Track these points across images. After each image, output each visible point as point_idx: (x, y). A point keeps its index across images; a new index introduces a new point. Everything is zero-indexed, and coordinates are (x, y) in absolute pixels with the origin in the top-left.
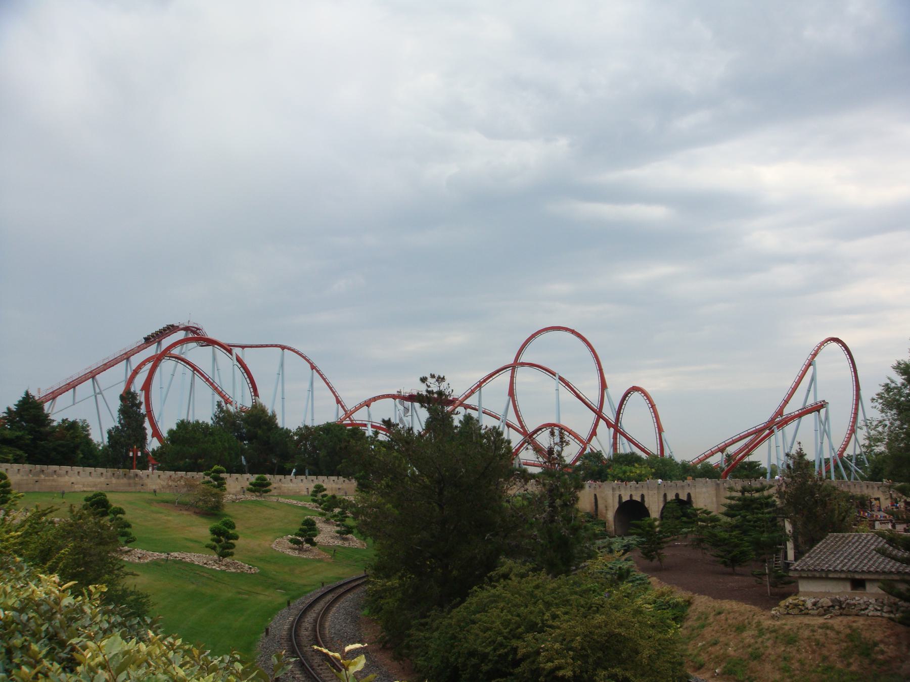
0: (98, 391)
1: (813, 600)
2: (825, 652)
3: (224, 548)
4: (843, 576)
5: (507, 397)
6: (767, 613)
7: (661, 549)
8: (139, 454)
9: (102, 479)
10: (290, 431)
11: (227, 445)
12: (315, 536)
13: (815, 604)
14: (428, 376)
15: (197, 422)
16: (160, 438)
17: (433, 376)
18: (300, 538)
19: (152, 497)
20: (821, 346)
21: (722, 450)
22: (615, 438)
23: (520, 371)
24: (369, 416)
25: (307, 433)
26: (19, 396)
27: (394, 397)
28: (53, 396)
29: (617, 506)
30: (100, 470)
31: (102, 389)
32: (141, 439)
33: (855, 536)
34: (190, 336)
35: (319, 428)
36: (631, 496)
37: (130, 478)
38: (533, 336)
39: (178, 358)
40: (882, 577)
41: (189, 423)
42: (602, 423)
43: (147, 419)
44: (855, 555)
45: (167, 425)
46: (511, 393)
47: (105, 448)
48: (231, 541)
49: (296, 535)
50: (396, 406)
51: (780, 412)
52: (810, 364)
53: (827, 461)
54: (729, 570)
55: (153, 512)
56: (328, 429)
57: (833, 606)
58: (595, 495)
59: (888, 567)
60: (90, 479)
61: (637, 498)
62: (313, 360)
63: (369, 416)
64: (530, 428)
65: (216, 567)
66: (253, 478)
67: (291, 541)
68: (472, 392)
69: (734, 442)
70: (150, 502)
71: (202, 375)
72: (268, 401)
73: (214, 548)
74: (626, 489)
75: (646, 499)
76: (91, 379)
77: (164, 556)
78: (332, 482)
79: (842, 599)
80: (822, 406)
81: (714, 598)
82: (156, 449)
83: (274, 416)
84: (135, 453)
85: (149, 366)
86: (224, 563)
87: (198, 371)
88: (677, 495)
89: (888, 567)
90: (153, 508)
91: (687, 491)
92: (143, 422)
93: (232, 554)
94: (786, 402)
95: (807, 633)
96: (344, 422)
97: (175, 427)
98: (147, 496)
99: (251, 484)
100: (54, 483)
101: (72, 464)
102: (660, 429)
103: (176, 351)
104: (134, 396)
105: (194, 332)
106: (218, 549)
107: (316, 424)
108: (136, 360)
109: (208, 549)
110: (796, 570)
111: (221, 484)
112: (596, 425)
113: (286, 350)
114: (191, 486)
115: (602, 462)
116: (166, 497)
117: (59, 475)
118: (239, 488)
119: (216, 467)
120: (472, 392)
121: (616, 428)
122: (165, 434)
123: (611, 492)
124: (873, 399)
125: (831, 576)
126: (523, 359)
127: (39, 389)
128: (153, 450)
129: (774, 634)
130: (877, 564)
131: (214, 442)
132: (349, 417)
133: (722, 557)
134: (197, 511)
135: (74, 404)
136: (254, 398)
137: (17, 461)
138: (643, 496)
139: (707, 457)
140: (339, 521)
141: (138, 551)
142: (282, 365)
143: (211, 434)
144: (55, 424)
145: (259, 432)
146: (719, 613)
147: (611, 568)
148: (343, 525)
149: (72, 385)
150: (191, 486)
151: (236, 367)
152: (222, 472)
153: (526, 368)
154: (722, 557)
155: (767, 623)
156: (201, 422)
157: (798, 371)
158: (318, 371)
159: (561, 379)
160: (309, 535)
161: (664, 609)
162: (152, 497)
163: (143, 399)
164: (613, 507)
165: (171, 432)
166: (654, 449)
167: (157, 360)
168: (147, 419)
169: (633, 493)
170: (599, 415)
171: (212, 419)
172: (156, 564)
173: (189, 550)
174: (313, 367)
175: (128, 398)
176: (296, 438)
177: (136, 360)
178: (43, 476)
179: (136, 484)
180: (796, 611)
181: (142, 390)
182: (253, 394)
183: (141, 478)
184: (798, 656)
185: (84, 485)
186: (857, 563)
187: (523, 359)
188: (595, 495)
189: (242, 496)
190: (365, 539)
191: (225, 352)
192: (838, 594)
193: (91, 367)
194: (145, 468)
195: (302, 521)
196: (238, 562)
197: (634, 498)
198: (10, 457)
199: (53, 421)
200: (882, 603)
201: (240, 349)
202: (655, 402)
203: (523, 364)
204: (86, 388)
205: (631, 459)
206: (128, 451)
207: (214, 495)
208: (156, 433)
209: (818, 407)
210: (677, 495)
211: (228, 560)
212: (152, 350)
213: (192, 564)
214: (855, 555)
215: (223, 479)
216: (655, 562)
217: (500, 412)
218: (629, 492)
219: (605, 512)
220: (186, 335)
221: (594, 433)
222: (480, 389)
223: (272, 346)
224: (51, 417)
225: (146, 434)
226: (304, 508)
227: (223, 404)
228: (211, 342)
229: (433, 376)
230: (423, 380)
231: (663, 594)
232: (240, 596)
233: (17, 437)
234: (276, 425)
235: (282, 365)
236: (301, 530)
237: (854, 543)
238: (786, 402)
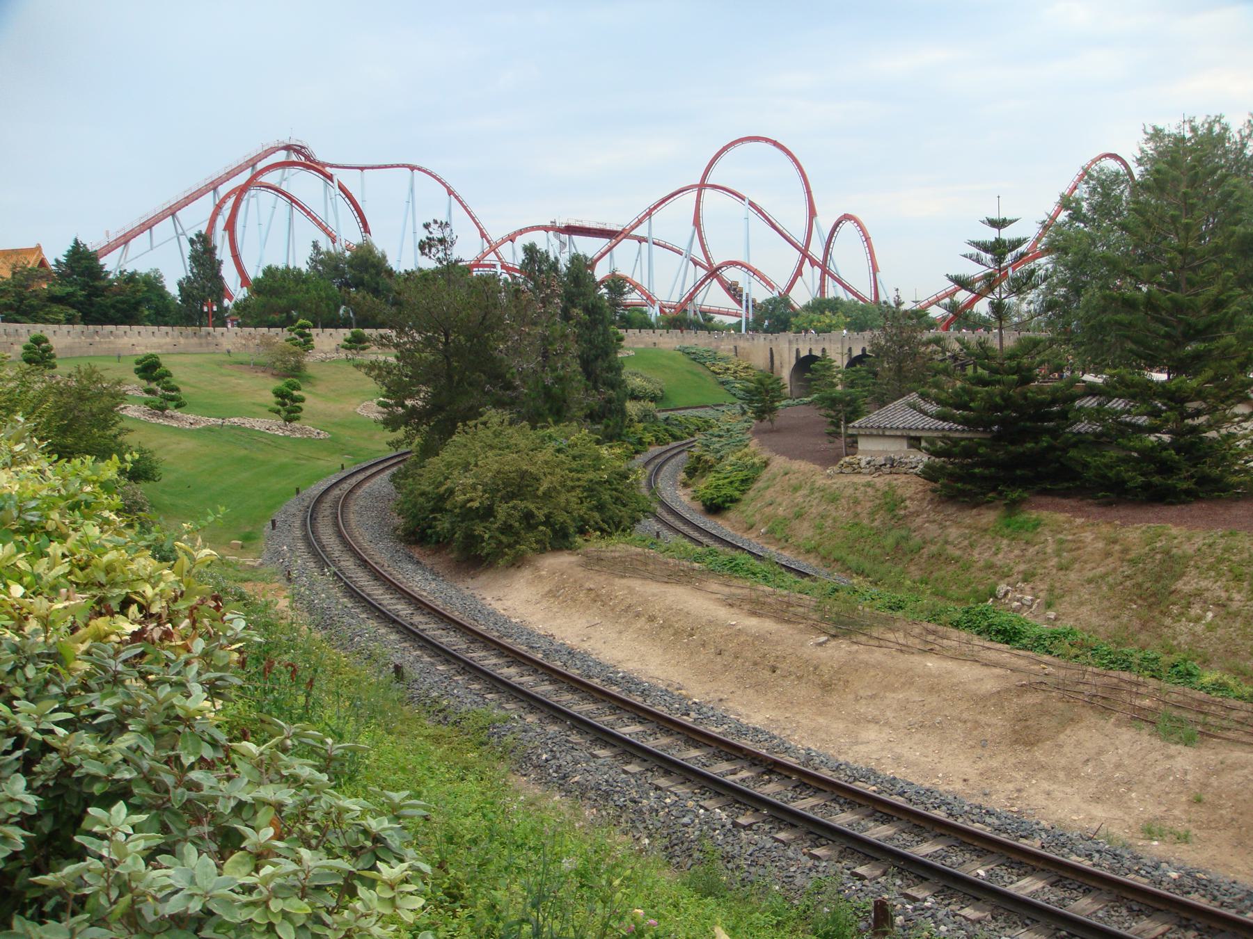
0: (180, 231)
1: (869, 459)
2: (859, 510)
3: (289, 412)
4: (899, 433)
5: (692, 228)
8: (215, 308)
9: (168, 340)
11: (323, 294)
13: (868, 463)
14: (431, 222)
19: (226, 358)
22: (822, 280)
23: (707, 193)
26: (68, 246)
27: (546, 229)
29: (794, 362)
30: (164, 329)
31: (185, 228)
36: (810, 350)
37: (201, 337)
38: (725, 149)
42: (807, 260)
46: (697, 222)
48: (297, 404)
49: (384, 397)
50: (548, 240)
55: (222, 375)
57: (885, 465)
60: (154, 340)
62: (449, 182)
65: (280, 433)
66: (346, 333)
67: (379, 404)
68: (640, 222)
70: (221, 364)
71: (302, 208)
73: (278, 412)
74: (804, 341)
77: (220, 422)
86: (289, 428)
90: (223, 371)
93: (298, 419)
95: (849, 491)
98: (217, 357)
99: (345, 340)
100: (111, 346)
101: (138, 323)
102: (875, 269)
106: (284, 414)
108: (224, 190)
109: (271, 414)
111: (307, 343)
112: (802, 263)
113: (415, 171)
114: (267, 344)
116: (241, 358)
117: (117, 336)
118: (334, 346)
119: (301, 321)
125: (887, 433)
126: (710, 181)
127: (107, 233)
129: (822, 493)
131: (308, 291)
133: (832, 417)
134: (275, 372)
137: (70, 321)
138: (824, 350)
141: (191, 417)
142: (412, 190)
143: (304, 282)
145: (366, 277)
149: (148, 225)
150: (267, 344)
151: (339, 197)
152: (309, 327)
154: (832, 417)
155: (820, 481)
158: (456, 197)
159: (752, 204)
162: (226, 358)
164: (790, 361)
166: (867, 292)
167: (242, 191)
170: (805, 253)
172: (209, 429)
173: (253, 415)
174: (450, 192)
177: (224, 190)
178: (97, 338)
179: (208, 344)
180: (849, 470)
183: (215, 337)
184: (834, 514)
189: (335, 355)
192: (895, 452)
193: (190, 189)
194: (224, 325)
196: (307, 426)
197: (814, 353)
198: (61, 317)
201: (359, 171)
202: (871, 234)
205: (833, 306)
211: (296, 424)
213: (252, 429)
215: (309, 335)
216: (766, 424)
217: (682, 245)
218: (807, 345)
220: (288, 156)
223: (398, 166)
229: (435, 222)
230: (427, 226)
232: (297, 462)
233: (68, 294)
235: (412, 190)
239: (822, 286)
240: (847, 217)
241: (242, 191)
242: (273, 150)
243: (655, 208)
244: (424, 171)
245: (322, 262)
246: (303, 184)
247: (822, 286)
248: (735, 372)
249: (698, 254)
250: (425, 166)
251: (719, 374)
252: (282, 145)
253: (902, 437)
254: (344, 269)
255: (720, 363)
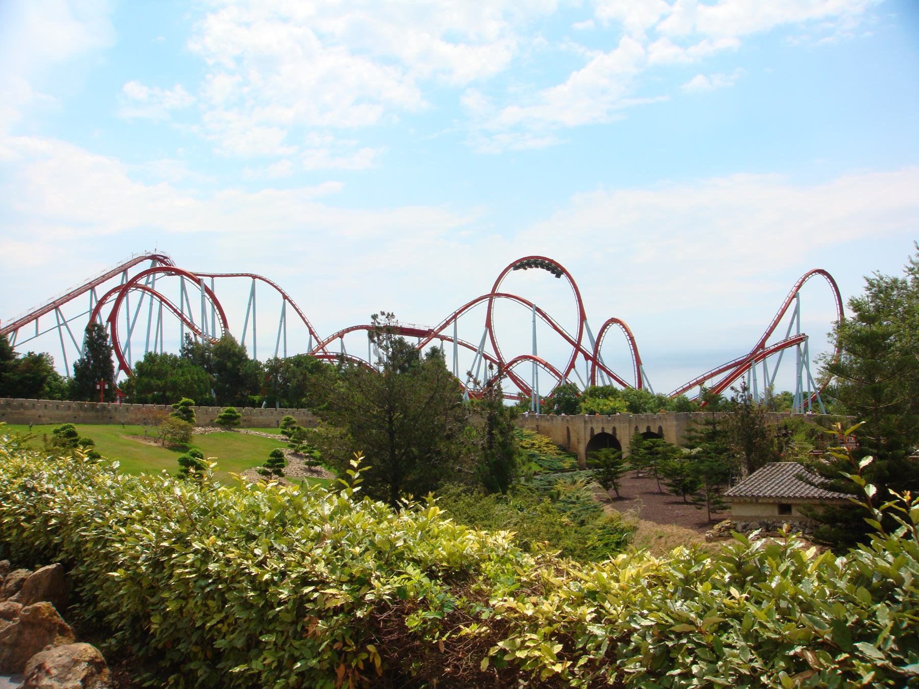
0: (61, 322)
1: (744, 523)
6: (703, 536)
7: (617, 478)
8: (107, 387)
10: (260, 363)
11: (196, 377)
12: (283, 466)
14: (379, 314)
15: (165, 354)
16: (128, 371)
17: (383, 314)
18: (269, 470)
20: (805, 278)
21: (700, 382)
22: (593, 370)
23: (497, 301)
24: (343, 346)
25: (276, 366)
28: (15, 327)
29: (588, 438)
32: (107, 371)
33: (791, 464)
34: (158, 266)
35: (288, 360)
36: (603, 429)
39: (145, 288)
40: (806, 502)
41: (156, 355)
42: (580, 355)
43: (113, 351)
44: (786, 482)
45: (136, 356)
46: (489, 325)
47: (71, 382)
51: (762, 345)
52: (794, 297)
53: (805, 395)
54: (681, 499)
56: (299, 361)
58: (568, 428)
59: (812, 492)
60: (58, 412)
61: (609, 431)
62: (284, 290)
63: (343, 346)
64: (507, 360)
68: (448, 323)
69: (712, 375)
72: (236, 333)
75: (618, 432)
76: (54, 311)
78: (302, 414)
79: (769, 522)
80: (801, 340)
81: (658, 523)
82: (123, 382)
83: (243, 348)
84: (102, 386)
85: (115, 296)
87: (166, 302)
88: (648, 428)
89: (812, 492)
91: (658, 424)
92: (110, 355)
94: (768, 335)
96: (317, 354)
97: (142, 360)
103: (142, 281)
104: (101, 328)
105: (162, 261)
107: (291, 354)
108: (101, 290)
110: (729, 496)
113: (215, 278)
115: (578, 395)
117: (26, 408)
119: (184, 400)
120: (448, 323)
121: (595, 360)
122: (133, 367)
123: (583, 424)
124: (829, 334)
128: (121, 382)
130: (803, 490)
132: (322, 348)
135: (37, 335)
136: (223, 329)
138: (614, 429)
139: (685, 390)
140: (308, 452)
143: (180, 366)
144: (20, 357)
146: (660, 537)
147: (570, 498)
148: (312, 456)
149: (34, 317)
153: (503, 299)
156: (169, 354)
157: (781, 304)
160: (278, 466)
161: (612, 534)
163: (109, 331)
164: (585, 439)
165: (139, 365)
166: (632, 382)
167: (123, 290)
168: (113, 351)
169: (605, 426)
170: (577, 347)
171: (180, 351)
174: (285, 297)
175: (93, 329)
176: (266, 370)
178: (9, 410)
181: (108, 320)
182: (222, 325)
183: (109, 411)
185: (51, 418)
186: (786, 489)
187: (499, 290)
188: (568, 428)
190: (329, 469)
191: (193, 282)
192: (767, 517)
195: (270, 453)
197: (607, 431)
199: (18, 354)
200: (805, 525)
202: (634, 335)
203: (499, 295)
204: (48, 320)
205: (608, 392)
206: (95, 384)
207: (182, 428)
208: (123, 366)
209: (800, 339)
210: (648, 428)
212: (117, 281)
214: (786, 482)
215: (191, 411)
219: (576, 444)
221: (572, 365)
222: (455, 320)
223: (242, 275)
224: (16, 350)
225: (114, 367)
226: (273, 440)
227: (192, 336)
228: (179, 272)
229: (383, 314)
231: (612, 521)
234: (246, 356)
236: (269, 461)
237: (787, 472)
238: (768, 335)
239: (593, 378)
240: (614, 320)
241: (123, 290)
242: (142, 259)
243: (460, 312)
244: (263, 280)
245: (190, 351)
246: (167, 285)
247: (593, 378)
248: (540, 447)
249: (489, 350)
250: (264, 276)
251: (527, 448)
252: (149, 255)
253: (774, 504)
254: (209, 356)
255: (527, 440)
